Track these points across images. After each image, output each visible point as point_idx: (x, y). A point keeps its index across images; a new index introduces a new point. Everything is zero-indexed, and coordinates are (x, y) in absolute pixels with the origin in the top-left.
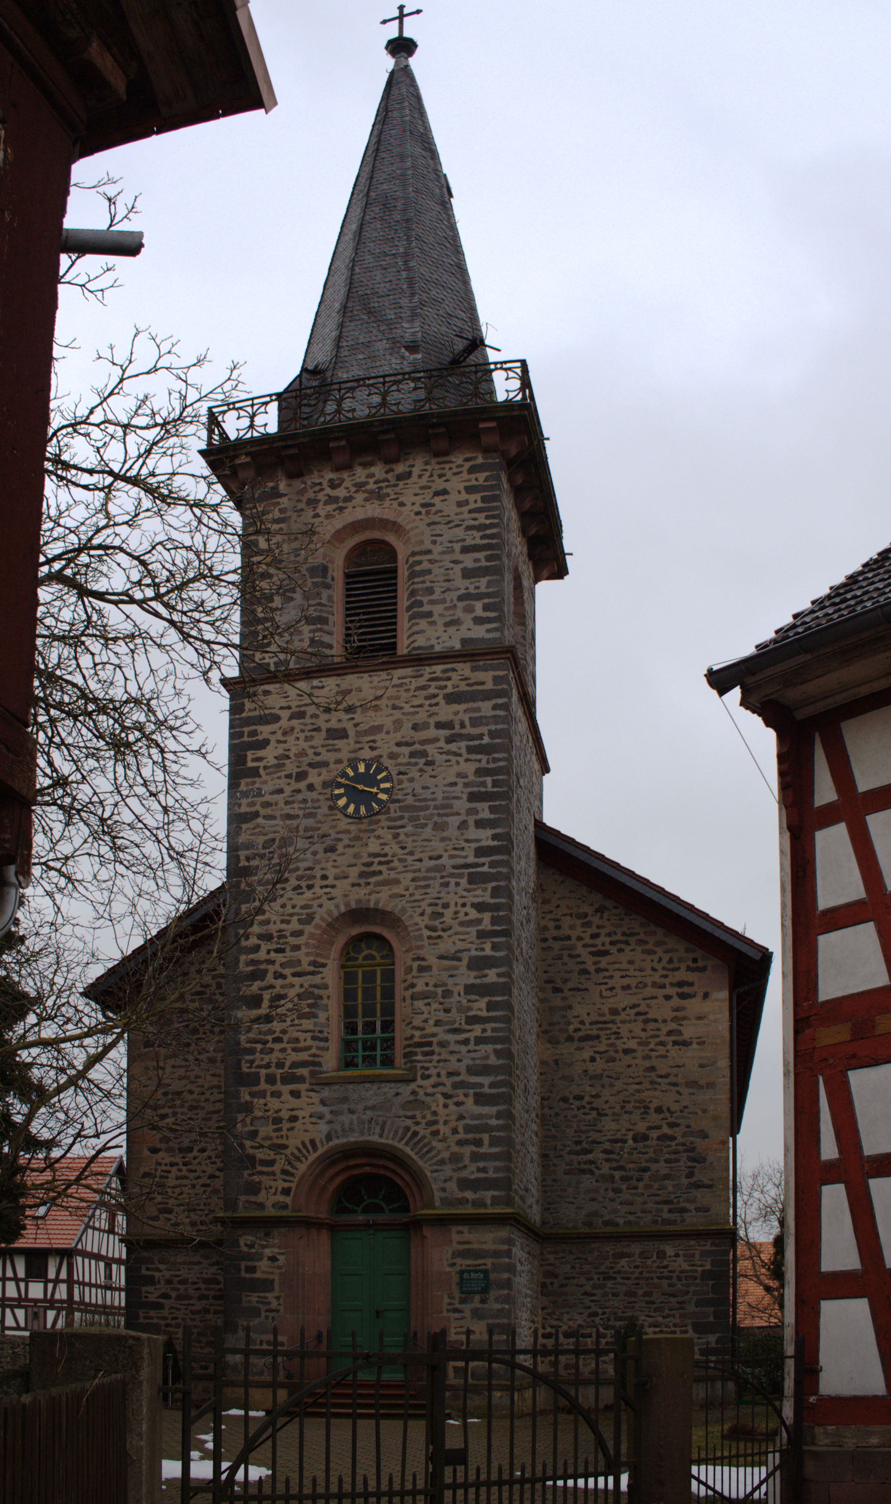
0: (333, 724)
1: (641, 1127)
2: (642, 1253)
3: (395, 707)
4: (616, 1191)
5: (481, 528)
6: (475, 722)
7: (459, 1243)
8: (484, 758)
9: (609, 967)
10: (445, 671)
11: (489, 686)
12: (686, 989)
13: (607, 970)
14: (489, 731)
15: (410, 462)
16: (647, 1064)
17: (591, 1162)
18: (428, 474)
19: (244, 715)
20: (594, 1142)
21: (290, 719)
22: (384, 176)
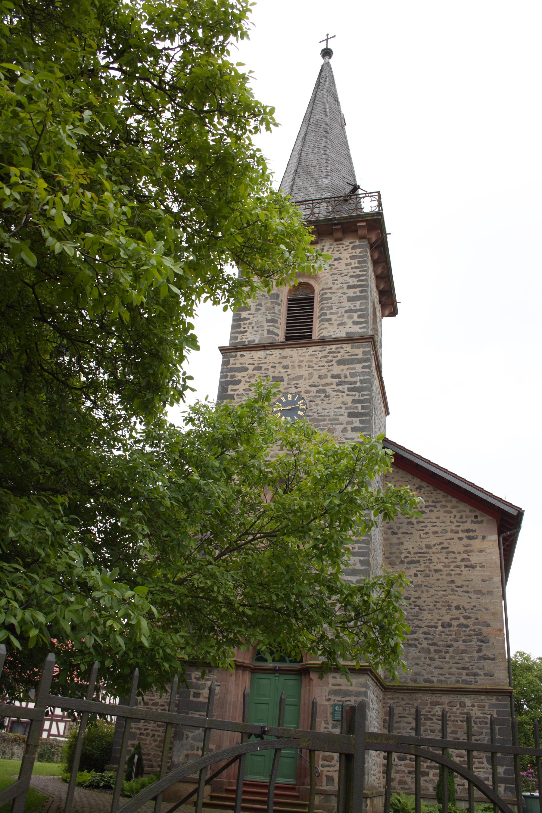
0: (276, 374)
1: (447, 618)
2: (450, 702)
3: (309, 366)
4: (432, 659)
5: (358, 276)
6: (352, 375)
7: (333, 685)
8: (357, 394)
9: (424, 520)
10: (337, 348)
11: (360, 356)
12: (471, 534)
13: (423, 522)
14: (360, 380)
15: (323, 244)
16: (449, 578)
17: (416, 640)
18: (331, 250)
19: (229, 366)
20: (417, 626)
21: (253, 370)
22: (317, 112)
